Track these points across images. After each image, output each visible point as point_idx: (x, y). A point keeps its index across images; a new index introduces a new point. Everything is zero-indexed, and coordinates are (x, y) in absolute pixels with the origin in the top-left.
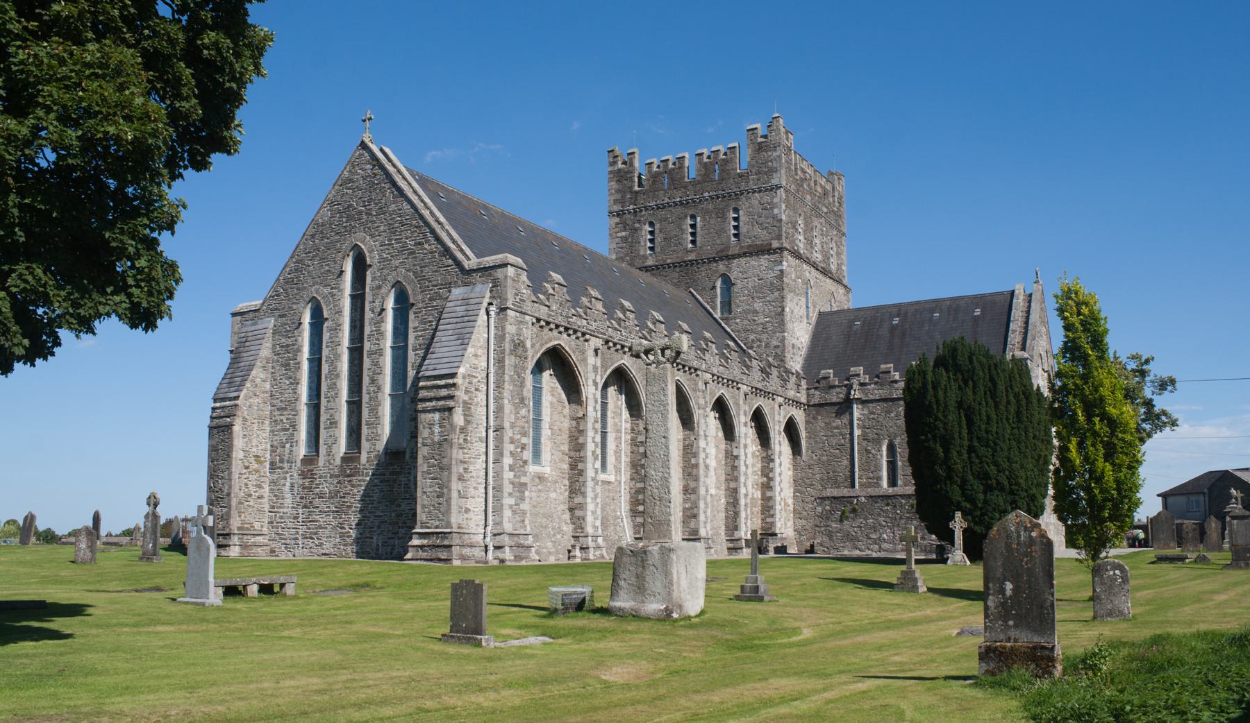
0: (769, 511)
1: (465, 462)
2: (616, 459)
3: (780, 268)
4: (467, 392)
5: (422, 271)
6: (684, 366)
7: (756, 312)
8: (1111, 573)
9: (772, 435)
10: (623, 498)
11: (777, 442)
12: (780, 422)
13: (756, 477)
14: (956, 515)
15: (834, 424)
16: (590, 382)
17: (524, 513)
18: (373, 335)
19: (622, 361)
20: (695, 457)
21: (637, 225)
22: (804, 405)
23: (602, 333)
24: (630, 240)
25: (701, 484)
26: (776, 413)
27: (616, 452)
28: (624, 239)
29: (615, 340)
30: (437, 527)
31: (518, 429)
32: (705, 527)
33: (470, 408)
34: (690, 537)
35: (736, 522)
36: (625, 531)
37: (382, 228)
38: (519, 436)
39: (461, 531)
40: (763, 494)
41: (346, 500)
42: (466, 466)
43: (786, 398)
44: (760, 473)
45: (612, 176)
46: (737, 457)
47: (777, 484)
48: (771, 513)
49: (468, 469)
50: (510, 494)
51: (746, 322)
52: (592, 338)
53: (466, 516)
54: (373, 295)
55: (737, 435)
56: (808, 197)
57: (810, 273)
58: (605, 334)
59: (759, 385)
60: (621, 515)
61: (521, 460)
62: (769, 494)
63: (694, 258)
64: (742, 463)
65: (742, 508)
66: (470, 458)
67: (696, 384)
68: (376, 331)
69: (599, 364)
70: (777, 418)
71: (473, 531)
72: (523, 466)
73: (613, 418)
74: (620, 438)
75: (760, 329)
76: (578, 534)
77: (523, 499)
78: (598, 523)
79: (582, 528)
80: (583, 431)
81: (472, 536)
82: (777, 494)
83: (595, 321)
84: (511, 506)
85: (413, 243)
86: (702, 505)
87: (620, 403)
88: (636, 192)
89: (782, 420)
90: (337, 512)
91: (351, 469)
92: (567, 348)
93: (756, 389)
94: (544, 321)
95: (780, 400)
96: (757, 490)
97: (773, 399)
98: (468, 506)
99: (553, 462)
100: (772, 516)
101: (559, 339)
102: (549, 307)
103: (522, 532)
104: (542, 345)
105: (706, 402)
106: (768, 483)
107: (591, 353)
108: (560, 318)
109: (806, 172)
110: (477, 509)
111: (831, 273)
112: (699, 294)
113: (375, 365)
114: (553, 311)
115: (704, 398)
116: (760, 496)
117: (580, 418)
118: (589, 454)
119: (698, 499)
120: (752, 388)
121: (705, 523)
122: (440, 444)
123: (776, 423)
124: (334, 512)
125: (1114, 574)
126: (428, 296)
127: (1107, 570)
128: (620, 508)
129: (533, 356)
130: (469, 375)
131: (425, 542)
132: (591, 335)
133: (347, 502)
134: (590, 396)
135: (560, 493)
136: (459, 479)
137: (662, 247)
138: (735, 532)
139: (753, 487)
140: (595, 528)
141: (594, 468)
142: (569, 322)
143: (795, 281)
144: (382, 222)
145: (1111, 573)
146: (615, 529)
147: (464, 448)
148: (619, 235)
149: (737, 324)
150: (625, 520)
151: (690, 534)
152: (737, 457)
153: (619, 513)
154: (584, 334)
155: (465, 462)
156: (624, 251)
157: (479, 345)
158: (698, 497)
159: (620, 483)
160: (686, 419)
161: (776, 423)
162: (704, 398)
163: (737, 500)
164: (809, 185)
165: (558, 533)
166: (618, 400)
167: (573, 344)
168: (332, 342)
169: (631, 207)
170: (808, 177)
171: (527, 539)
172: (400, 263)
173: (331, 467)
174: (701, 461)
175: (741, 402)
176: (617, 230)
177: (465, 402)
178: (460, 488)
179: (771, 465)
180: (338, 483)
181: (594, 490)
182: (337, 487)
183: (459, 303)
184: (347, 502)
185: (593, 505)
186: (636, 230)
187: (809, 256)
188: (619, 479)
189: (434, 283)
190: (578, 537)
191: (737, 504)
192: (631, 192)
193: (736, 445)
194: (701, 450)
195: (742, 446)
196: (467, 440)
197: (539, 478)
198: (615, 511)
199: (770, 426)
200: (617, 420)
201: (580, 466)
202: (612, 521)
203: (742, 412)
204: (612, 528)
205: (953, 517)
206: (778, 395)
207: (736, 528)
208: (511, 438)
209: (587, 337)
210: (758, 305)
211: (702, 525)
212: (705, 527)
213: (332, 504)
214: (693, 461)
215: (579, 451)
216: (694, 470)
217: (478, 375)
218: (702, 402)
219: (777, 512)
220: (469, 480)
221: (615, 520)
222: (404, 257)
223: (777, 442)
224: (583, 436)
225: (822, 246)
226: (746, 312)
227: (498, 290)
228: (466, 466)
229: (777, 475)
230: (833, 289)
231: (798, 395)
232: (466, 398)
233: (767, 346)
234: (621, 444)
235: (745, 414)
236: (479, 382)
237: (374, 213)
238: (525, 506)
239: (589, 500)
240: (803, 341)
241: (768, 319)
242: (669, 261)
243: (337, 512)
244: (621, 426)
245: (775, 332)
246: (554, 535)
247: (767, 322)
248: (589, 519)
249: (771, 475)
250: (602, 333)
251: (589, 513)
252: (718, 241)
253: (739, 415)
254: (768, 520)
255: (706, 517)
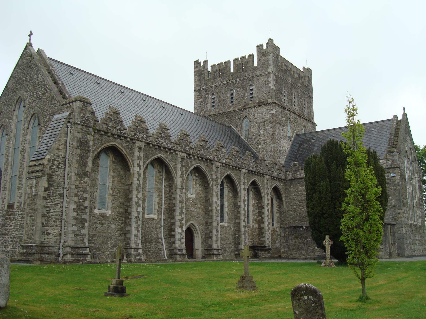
0: (262, 235)
1: (48, 207)
2: (159, 207)
3: (272, 112)
4: (51, 168)
5: (44, 107)
6: (202, 158)
7: (260, 135)
8: (306, 298)
9: (263, 195)
10: (162, 228)
11: (266, 199)
12: (267, 188)
13: (255, 217)
14: (326, 237)
15: (299, 190)
16: (136, 165)
17: (84, 235)
18: (23, 142)
19: (160, 155)
20: (211, 206)
21: (207, 96)
22: (284, 180)
23: (145, 139)
24: (203, 103)
25: (214, 220)
26: (265, 184)
27: (158, 203)
28: (201, 102)
29: (154, 144)
30: (31, 243)
31: (81, 189)
32: (217, 244)
33: (53, 177)
34: (208, 249)
35: (239, 240)
36: (163, 245)
37: (30, 88)
38: (82, 193)
39: (43, 245)
40: (259, 226)
41: (8, 228)
42: (48, 209)
43: (271, 177)
44: (257, 215)
45: (196, 73)
46: (240, 206)
47: (266, 220)
48: (264, 235)
49: (50, 211)
50: (74, 225)
51: (256, 140)
52: (137, 142)
53: (47, 237)
54: (25, 121)
55: (240, 195)
56: (289, 79)
57: (290, 115)
58: (148, 140)
59: (254, 169)
60: (161, 237)
61: (83, 206)
62: (262, 226)
63: (232, 110)
64: (242, 209)
65: (243, 233)
66: (52, 205)
67: (212, 168)
68: (25, 139)
69: (142, 155)
70: (266, 186)
71: (52, 245)
72: (84, 210)
73: (157, 185)
74: (162, 195)
75: (263, 143)
76: (127, 247)
77: (83, 228)
78: (139, 241)
79: (129, 244)
80: (131, 191)
81: (50, 248)
82: (266, 225)
83: (140, 133)
84: (74, 232)
85: (41, 93)
86: (214, 231)
87: (161, 177)
88: (206, 80)
89: (269, 187)
90: (4, 234)
91: (10, 212)
92: (120, 147)
93: (252, 171)
94: (103, 131)
95: (268, 177)
96: (255, 223)
97: (264, 177)
98: (49, 231)
99: (113, 208)
100: (264, 237)
101: (114, 141)
102: (107, 124)
103: (82, 245)
104: (101, 145)
105: (217, 178)
106: (262, 220)
107: (136, 149)
108: (114, 131)
109: (288, 67)
110: (56, 233)
111: (304, 115)
112: (235, 127)
113: (23, 157)
114: (109, 127)
115: (216, 175)
116: (257, 227)
117: (130, 184)
118: (134, 203)
119: (212, 228)
120: (249, 171)
121: (217, 241)
122: (35, 196)
123: (265, 189)
124: (3, 234)
125: (308, 298)
126: (46, 120)
127: (302, 295)
128: (161, 233)
129: (94, 151)
130: (52, 160)
131: (25, 251)
132: (136, 140)
133: (8, 229)
134: (136, 173)
135: (118, 225)
136: (43, 216)
137: (218, 106)
138: (239, 246)
139: (253, 222)
140: (137, 244)
141: (137, 211)
142: (121, 133)
143: (281, 119)
144: (31, 85)
145: (306, 298)
146: (157, 244)
147: (48, 199)
148: (199, 101)
149: (252, 141)
150: (163, 239)
151: (208, 247)
152: (240, 206)
153: (160, 236)
154: (131, 139)
155: (48, 207)
156: (201, 108)
157: (61, 143)
158: (213, 227)
159: (161, 219)
160: (207, 186)
161: (265, 189)
162: (216, 175)
163: (240, 229)
164: (290, 73)
165: (115, 247)
166: (161, 175)
167: (124, 145)
168: (8, 146)
169: (204, 87)
170: (289, 69)
171: (86, 250)
172: (36, 104)
173: (3, 211)
174: (214, 208)
175: (242, 178)
176: (198, 98)
177: (49, 174)
178: (43, 221)
179: (263, 210)
180: (5, 219)
181: (136, 223)
182: (5, 221)
183: (55, 122)
184: (8, 229)
185: (136, 231)
186: (206, 98)
187: (290, 107)
188: (160, 217)
189: (48, 113)
190: (127, 249)
191: (240, 231)
192: (204, 80)
193: (239, 200)
194: (214, 202)
195: (242, 200)
196: (50, 195)
197: (103, 217)
198: (157, 235)
199: (262, 190)
200: (160, 186)
201: (129, 210)
202: (154, 240)
203: (242, 183)
204: (154, 244)
205: (324, 238)
206: (266, 175)
207: (239, 244)
208: (75, 194)
209: (134, 141)
210: (261, 132)
211: (214, 242)
212: (217, 244)
213: (3, 230)
214: (210, 208)
215: (129, 202)
216: (211, 213)
217: (59, 160)
218: (215, 177)
219: (266, 235)
220: (50, 217)
221: (156, 240)
222: (38, 101)
223: (266, 199)
224: (131, 194)
225: (299, 103)
226: (256, 135)
227: (73, 115)
228: (48, 209)
229: (266, 216)
230: (305, 124)
231: (280, 175)
232: (50, 172)
233: (266, 151)
234: (162, 199)
235: (244, 184)
236: (60, 163)
237: (28, 80)
238: (85, 232)
239: (133, 229)
240: (286, 148)
241: (266, 138)
242: (221, 112)
243: (4, 234)
244: (162, 189)
245: (270, 144)
246: (111, 248)
247: (266, 139)
248: (133, 239)
249: (263, 216)
250: (145, 139)
251: (133, 236)
252: (243, 101)
253: (240, 185)
254: (262, 239)
255: (217, 238)
